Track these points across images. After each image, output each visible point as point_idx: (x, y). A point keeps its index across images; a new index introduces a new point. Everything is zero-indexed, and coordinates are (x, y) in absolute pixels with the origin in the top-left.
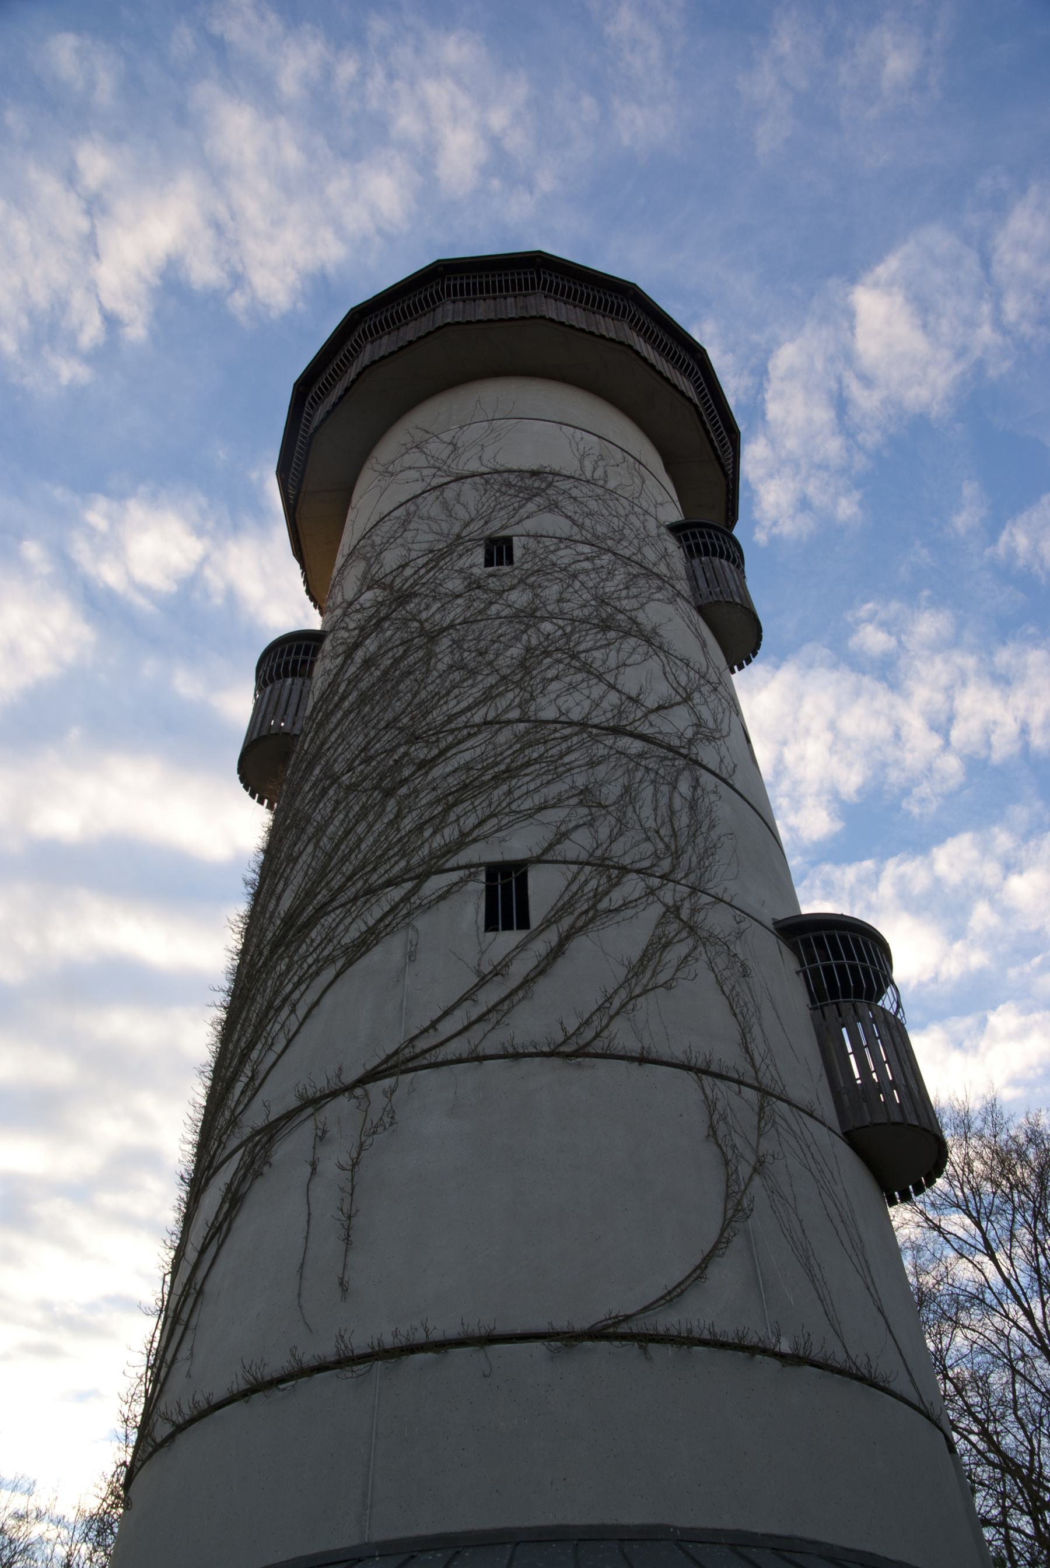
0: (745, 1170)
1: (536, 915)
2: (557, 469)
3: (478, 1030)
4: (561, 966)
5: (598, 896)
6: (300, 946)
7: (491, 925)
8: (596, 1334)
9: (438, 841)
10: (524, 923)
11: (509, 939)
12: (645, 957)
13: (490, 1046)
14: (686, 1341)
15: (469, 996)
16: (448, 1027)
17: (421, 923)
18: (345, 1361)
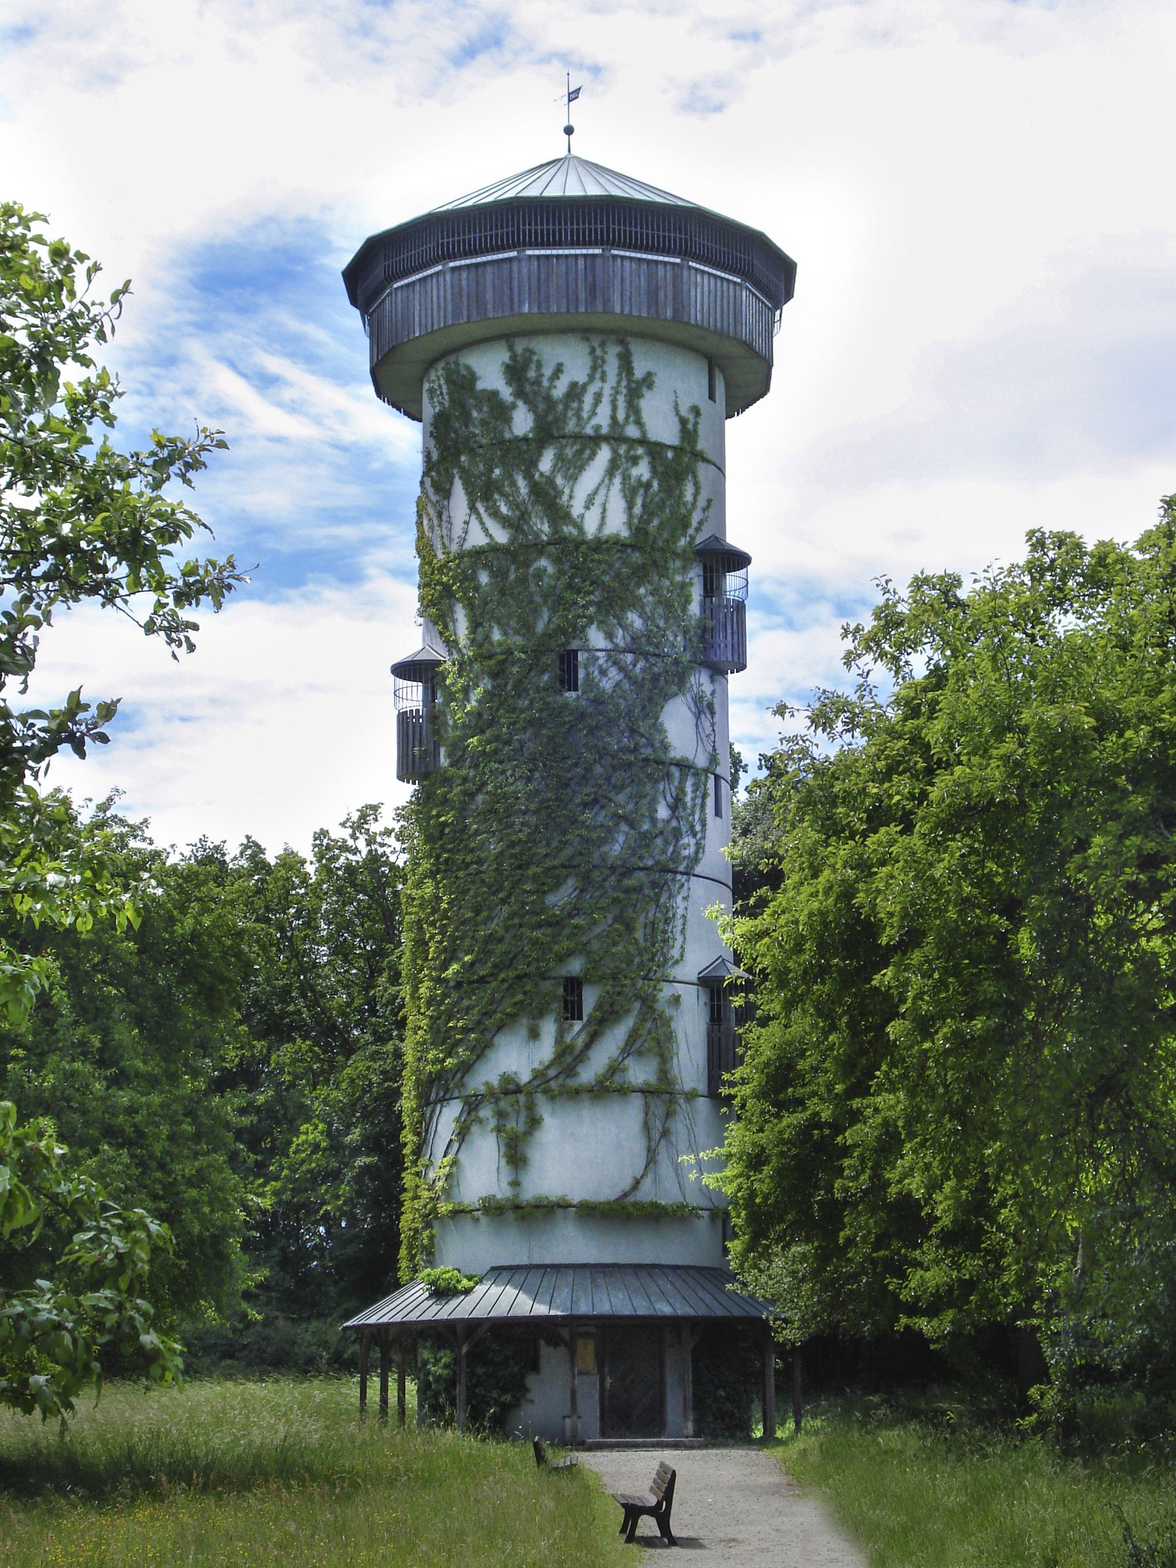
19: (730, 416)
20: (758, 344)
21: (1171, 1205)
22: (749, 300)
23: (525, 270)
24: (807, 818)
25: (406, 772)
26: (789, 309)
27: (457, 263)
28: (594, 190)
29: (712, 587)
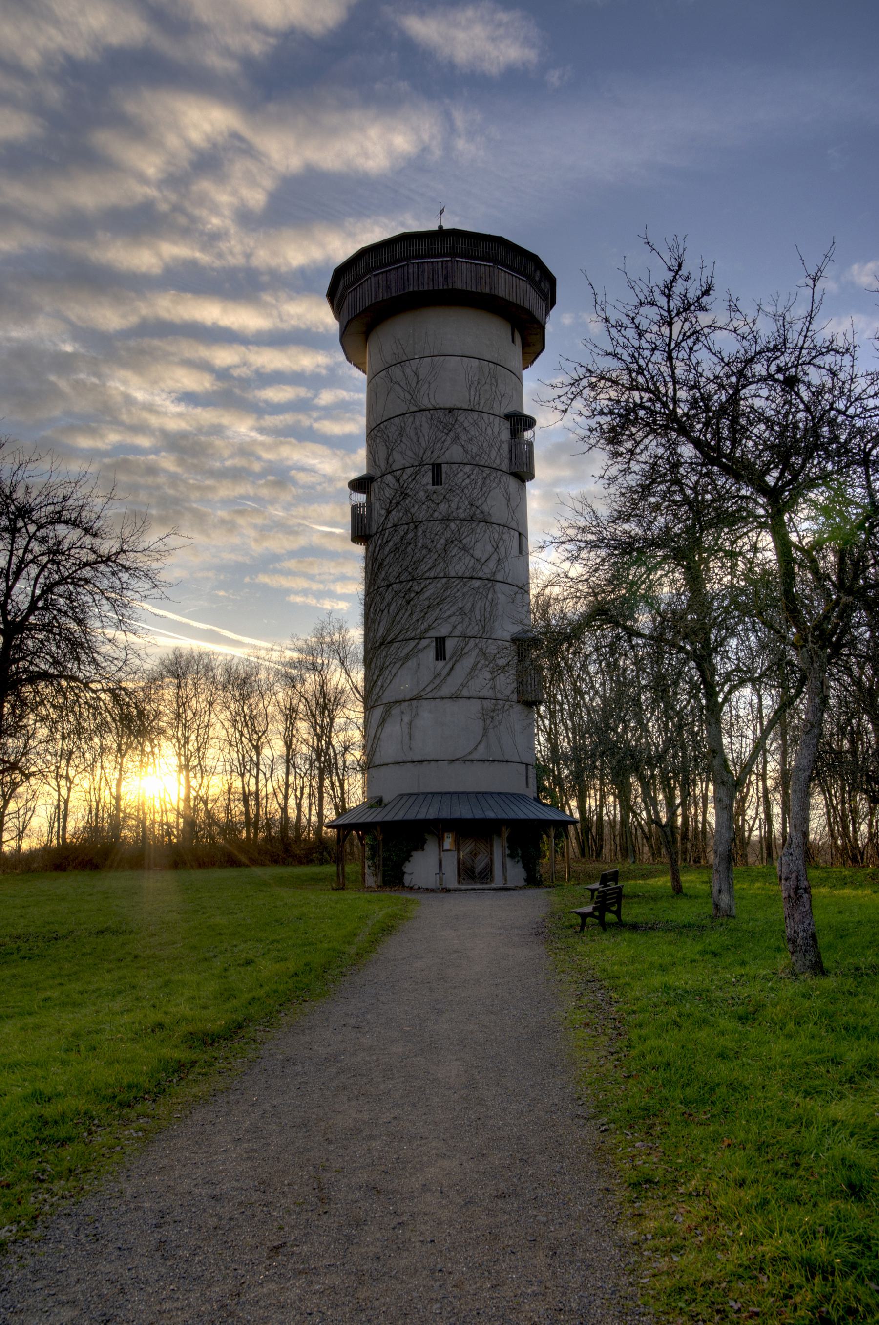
1: (447, 657)
5: (462, 649)
6: (743, 527)
7: (437, 659)
8: (457, 760)
9: (423, 627)
10: (445, 659)
11: (441, 663)
13: (437, 696)
15: (431, 682)
17: (420, 655)
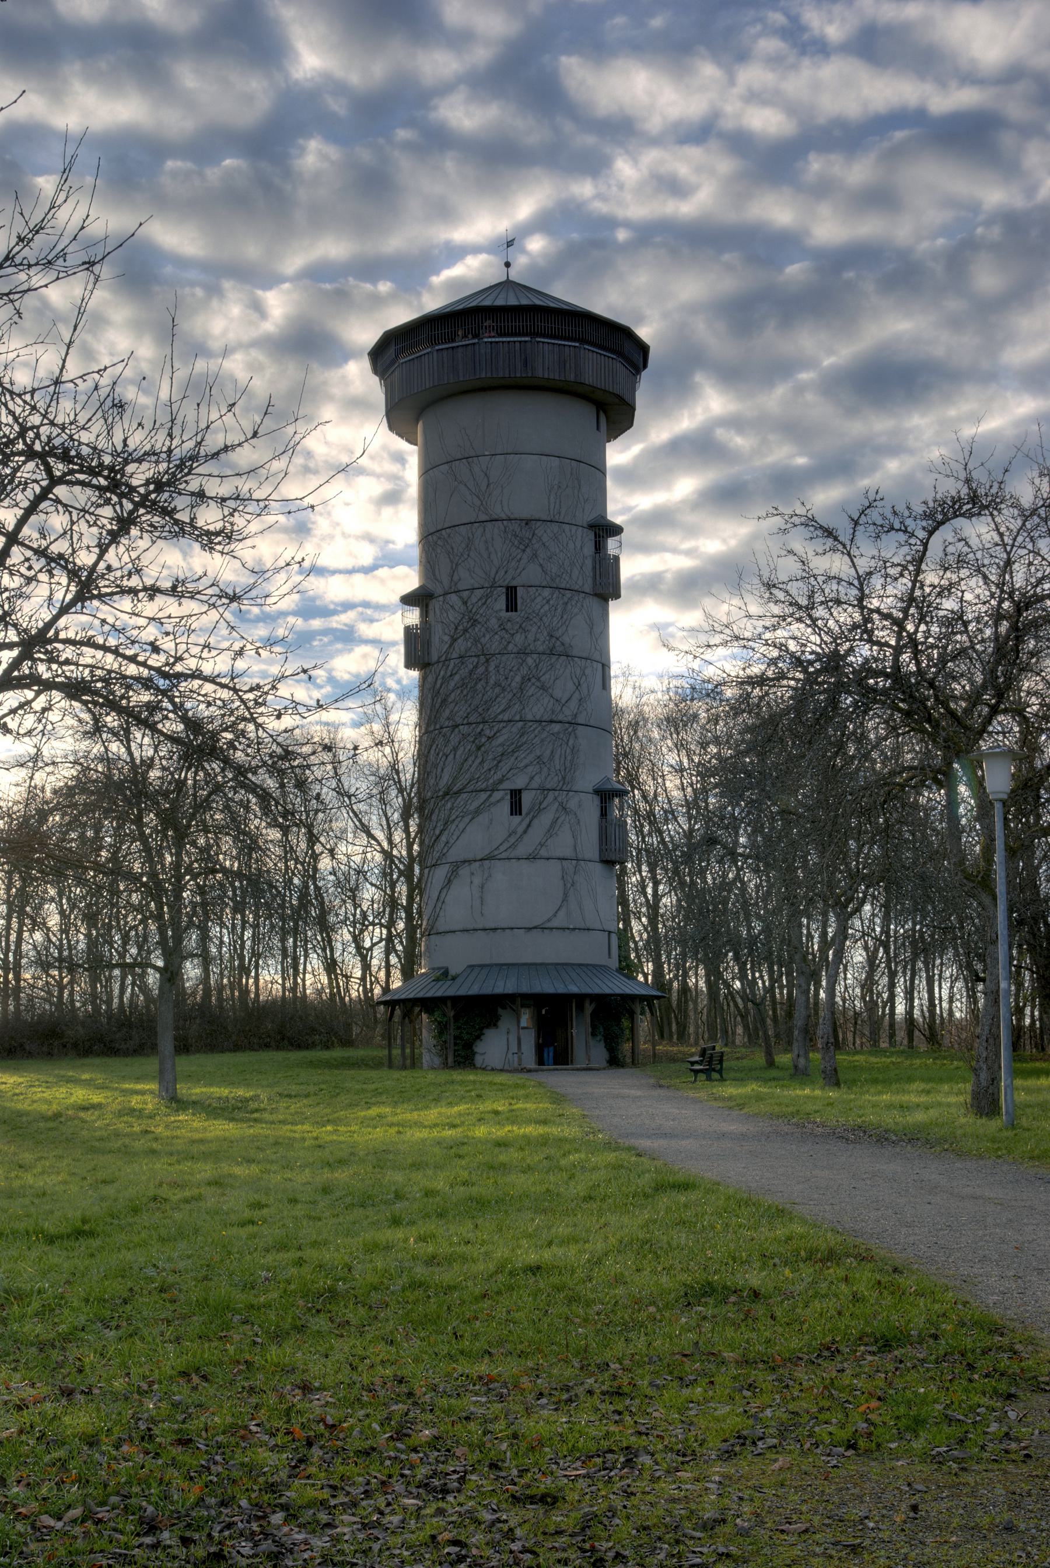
0: (569, 885)
2: (861, 508)
3: (510, 850)
4: (530, 830)
7: (512, 814)
11: (517, 819)
12: (551, 827)
13: (512, 856)
14: (552, 929)
15: (506, 840)
16: (502, 848)
18: (485, 930)
19: (609, 441)
20: (627, 398)
21: (1029, 743)
22: (619, 367)
23: (483, 351)
24: (756, 700)
25: (411, 662)
26: (644, 374)
27: (440, 347)
28: (524, 302)
29: (599, 547)
